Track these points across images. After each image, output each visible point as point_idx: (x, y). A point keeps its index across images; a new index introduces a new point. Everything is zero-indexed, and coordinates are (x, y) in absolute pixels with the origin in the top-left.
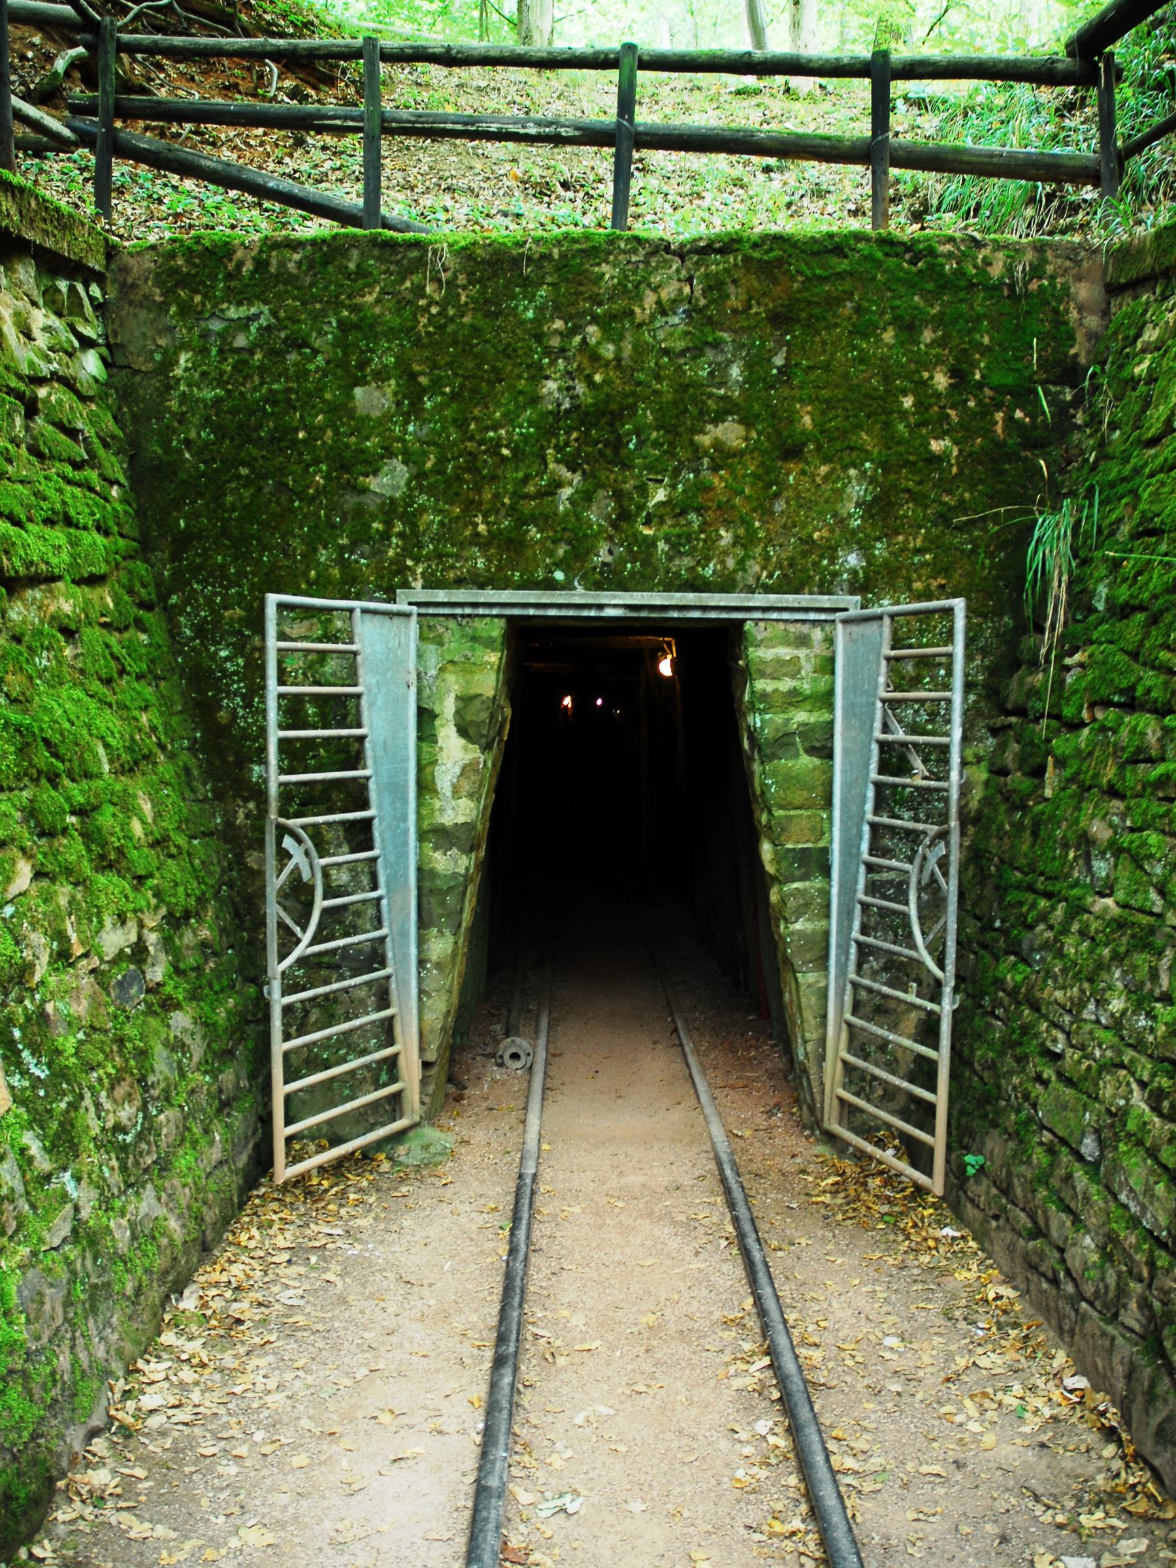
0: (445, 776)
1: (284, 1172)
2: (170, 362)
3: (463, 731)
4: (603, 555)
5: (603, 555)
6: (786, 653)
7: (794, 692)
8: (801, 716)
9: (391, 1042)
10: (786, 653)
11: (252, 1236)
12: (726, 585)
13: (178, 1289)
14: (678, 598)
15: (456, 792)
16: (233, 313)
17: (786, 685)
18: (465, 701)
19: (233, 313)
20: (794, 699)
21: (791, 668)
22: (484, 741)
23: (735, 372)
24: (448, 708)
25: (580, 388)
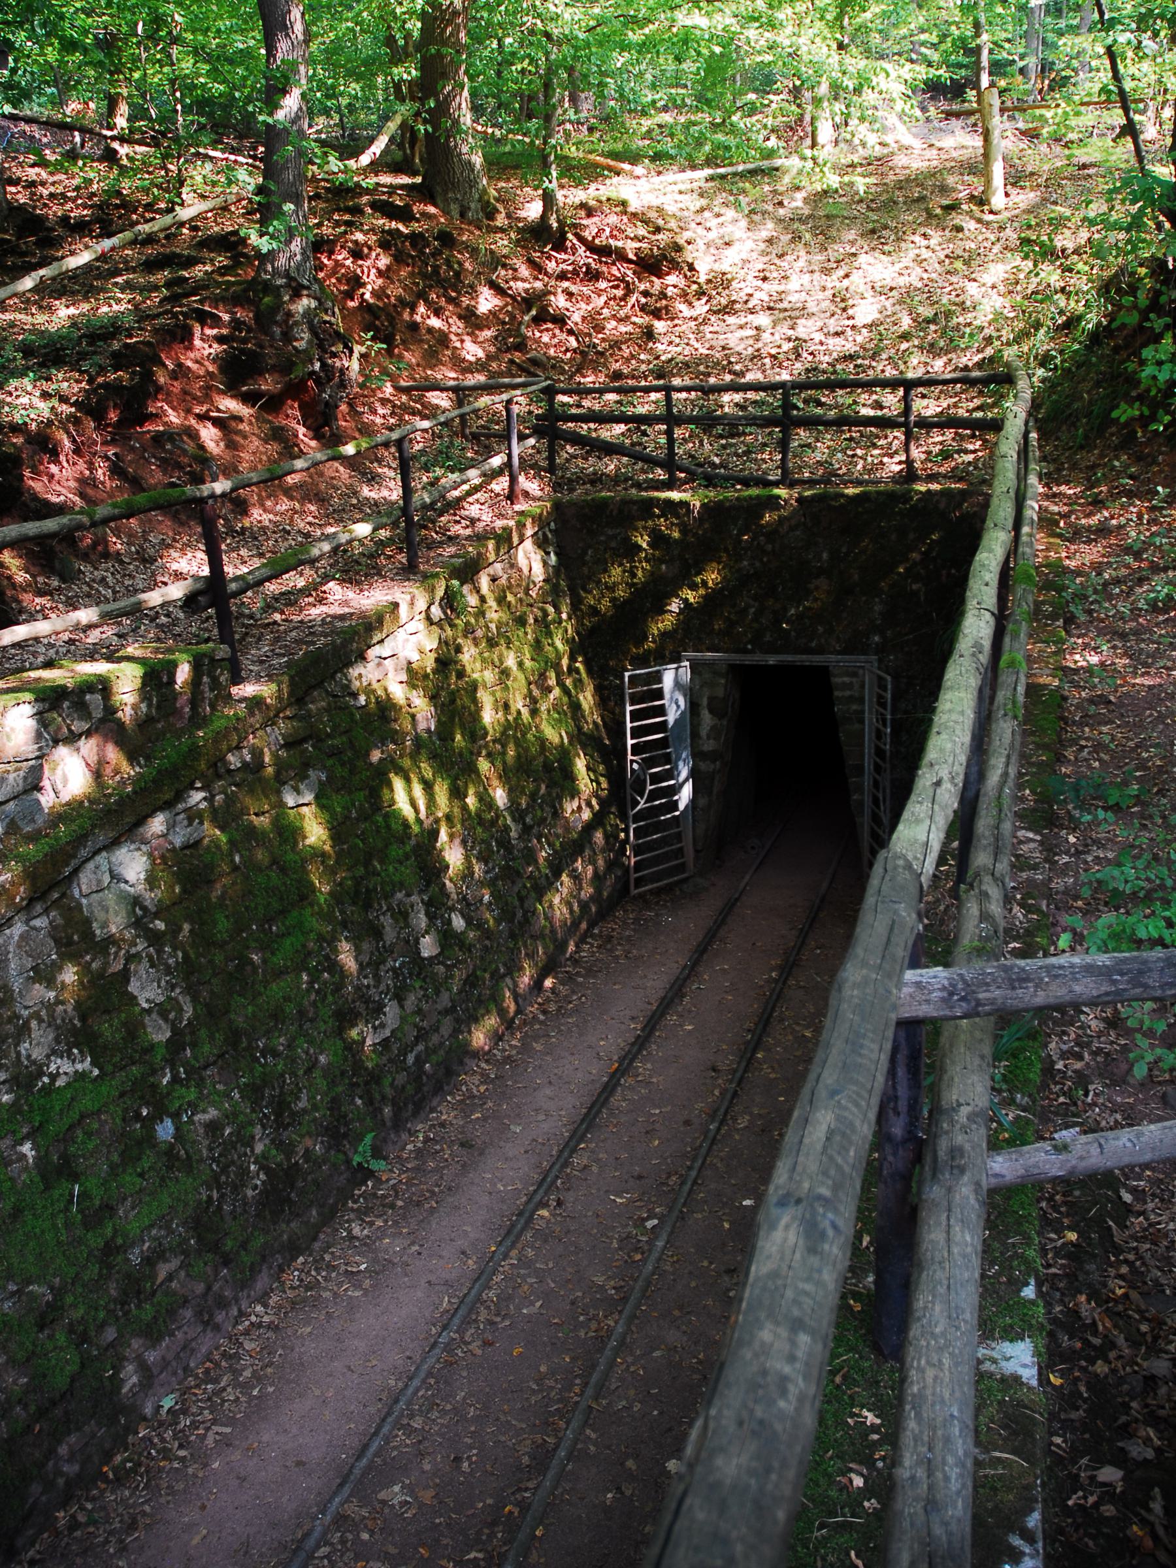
0: (704, 732)
1: (634, 892)
2: (585, 553)
3: (711, 712)
4: (768, 638)
5: (768, 638)
6: (847, 679)
7: (851, 697)
8: (854, 707)
9: (680, 841)
10: (847, 679)
11: (620, 913)
12: (820, 651)
13: (1110, 702)
14: (798, 657)
15: (709, 737)
16: (610, 532)
17: (848, 693)
18: (711, 699)
19: (610, 532)
20: (851, 699)
21: (849, 686)
22: (990, 437)
23: (825, 556)
24: (705, 702)
25: (758, 564)
